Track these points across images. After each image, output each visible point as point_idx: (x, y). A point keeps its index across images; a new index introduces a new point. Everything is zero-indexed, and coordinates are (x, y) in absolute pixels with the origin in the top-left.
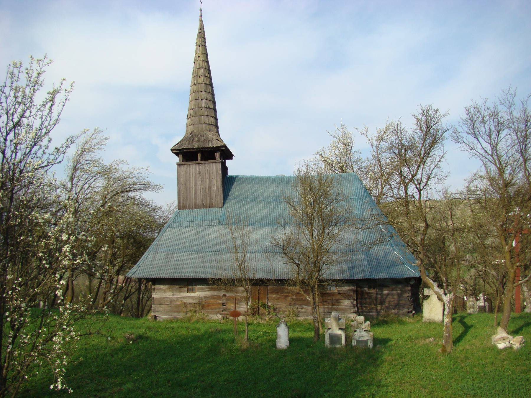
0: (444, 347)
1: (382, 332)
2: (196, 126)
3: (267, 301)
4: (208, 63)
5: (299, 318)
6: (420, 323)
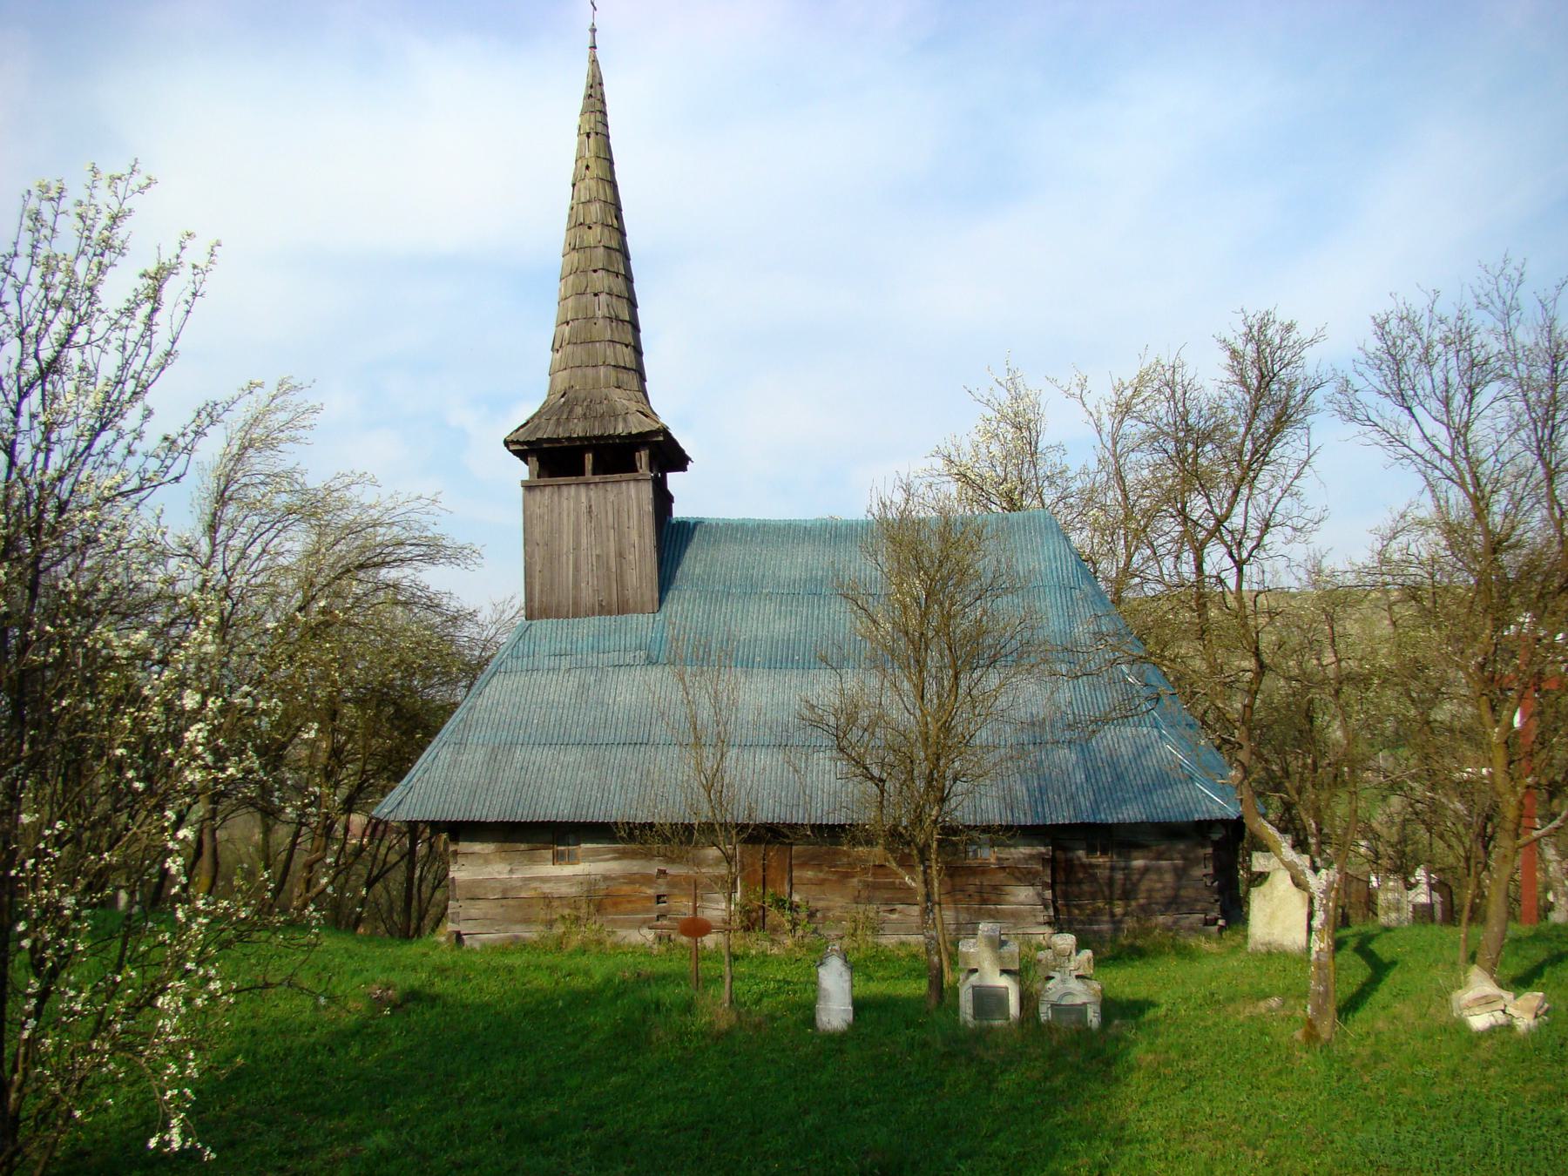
1: (1129, 981)
2: (579, 372)
3: (787, 888)
4: (613, 185)
5: (884, 941)
6: (1242, 956)
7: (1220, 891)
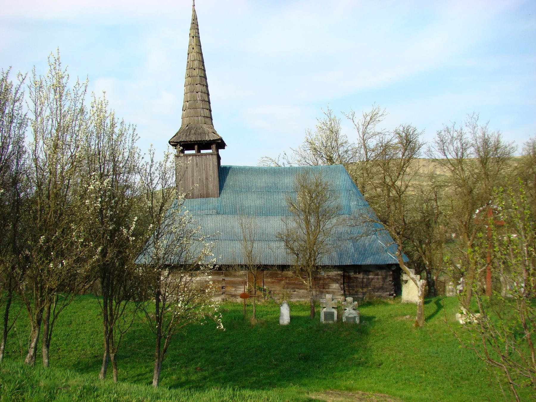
0: (417, 322)
1: (367, 311)
2: (192, 118)
3: (262, 284)
4: (201, 54)
5: (292, 300)
6: (400, 304)
7: (394, 285)
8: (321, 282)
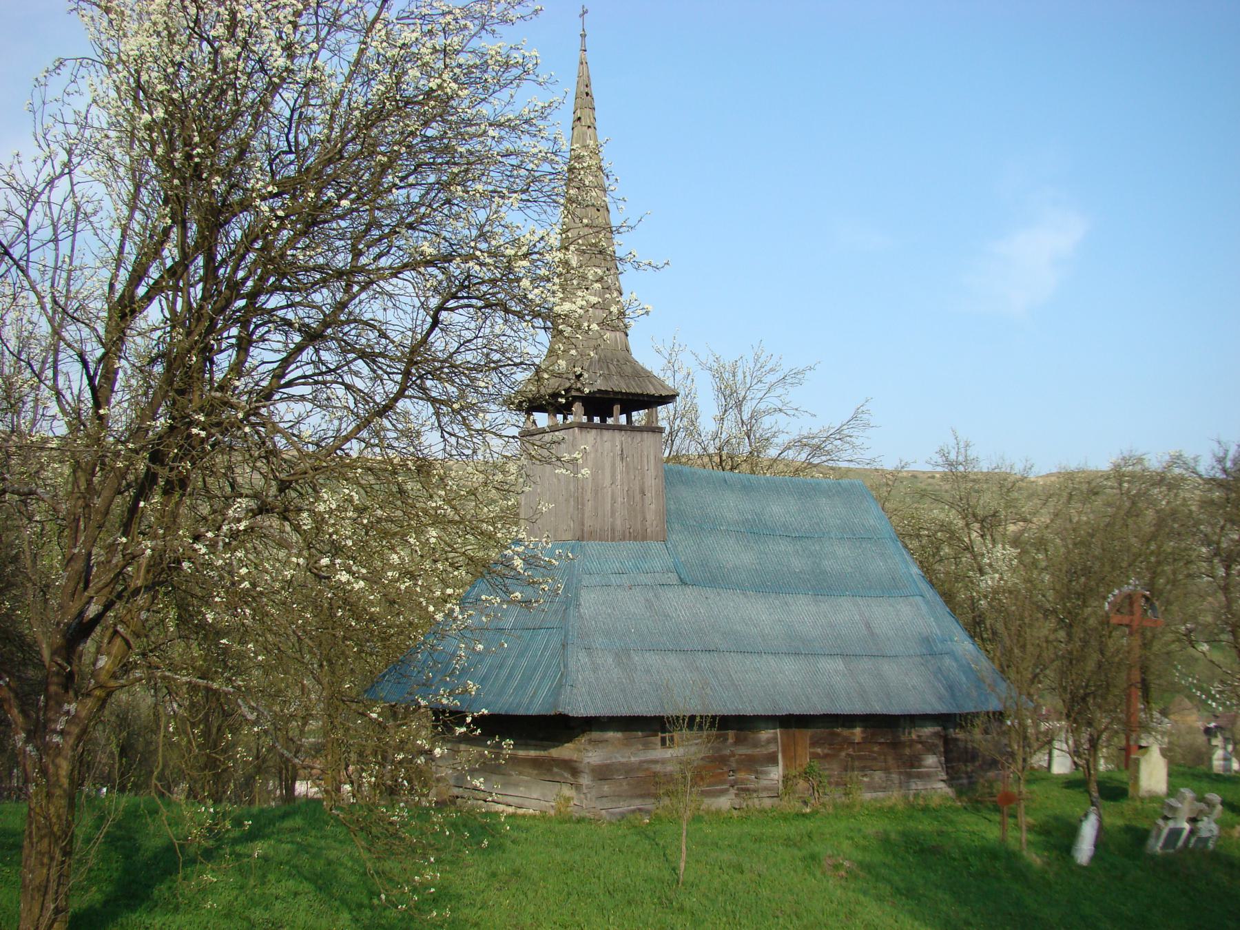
8: (907, 751)
